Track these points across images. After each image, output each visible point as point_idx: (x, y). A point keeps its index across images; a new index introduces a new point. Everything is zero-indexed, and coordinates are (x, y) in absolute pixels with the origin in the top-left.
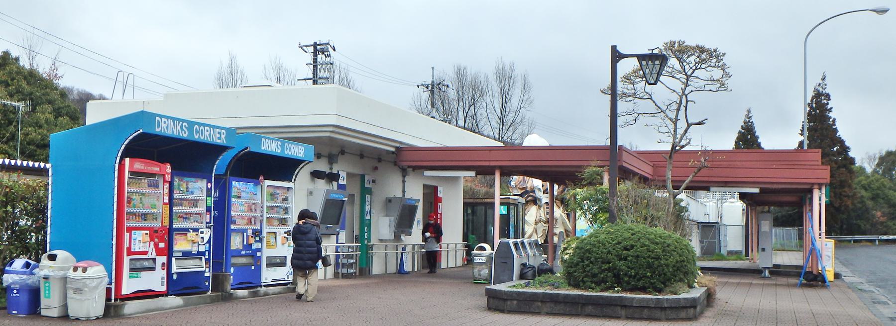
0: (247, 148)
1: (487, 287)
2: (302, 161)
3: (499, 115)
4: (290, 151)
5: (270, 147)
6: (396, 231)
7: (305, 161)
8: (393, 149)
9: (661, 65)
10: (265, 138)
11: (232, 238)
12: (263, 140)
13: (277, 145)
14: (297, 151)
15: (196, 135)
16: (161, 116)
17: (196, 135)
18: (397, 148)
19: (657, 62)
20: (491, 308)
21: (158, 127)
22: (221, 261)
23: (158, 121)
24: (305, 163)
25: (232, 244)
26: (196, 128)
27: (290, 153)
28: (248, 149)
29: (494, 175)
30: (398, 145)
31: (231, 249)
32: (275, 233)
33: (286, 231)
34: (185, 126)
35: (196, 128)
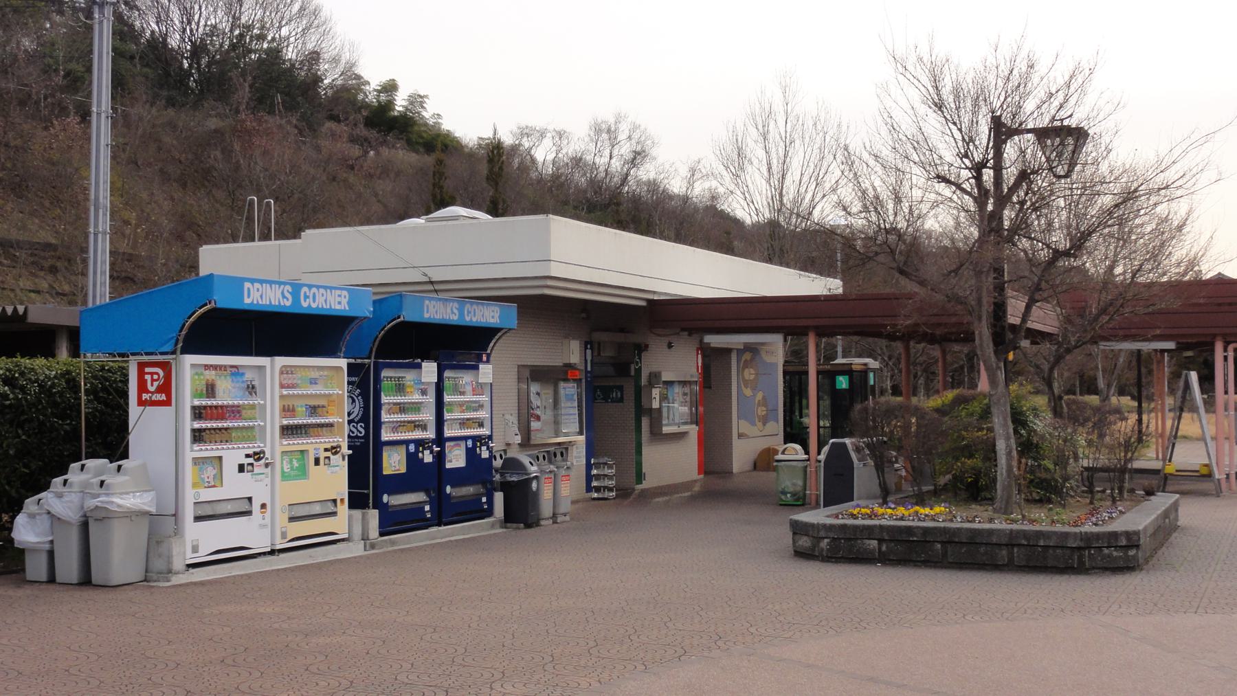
0: (399, 317)
1: (792, 517)
2: (499, 330)
3: (292, 14)
4: (314, 301)
5: (437, 312)
6: (1206, 396)
7: (501, 329)
8: (643, 303)
9: (1076, 146)
10: (431, 299)
11: (385, 455)
12: (427, 302)
13: (452, 310)
14: (488, 316)
15: (305, 301)
16: (253, 281)
17: (305, 301)
18: (649, 301)
19: (1070, 141)
20: (802, 554)
21: (249, 296)
22: (366, 491)
23: (249, 289)
24: (499, 334)
25: (385, 464)
26: (305, 293)
27: (314, 305)
28: (402, 319)
29: (807, 335)
30: (650, 297)
31: (385, 473)
32: (220, 458)
33: (250, 452)
34: (288, 291)
35: (305, 293)
